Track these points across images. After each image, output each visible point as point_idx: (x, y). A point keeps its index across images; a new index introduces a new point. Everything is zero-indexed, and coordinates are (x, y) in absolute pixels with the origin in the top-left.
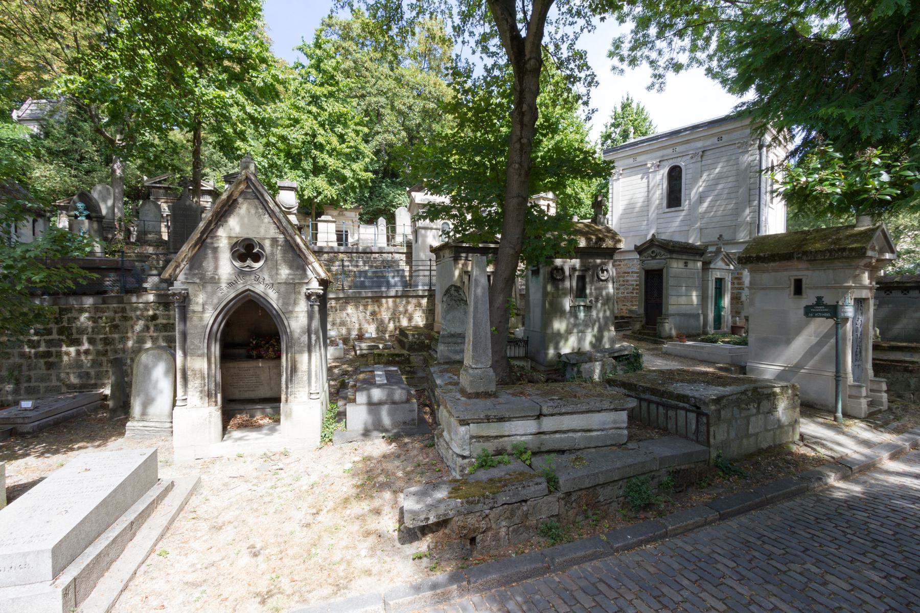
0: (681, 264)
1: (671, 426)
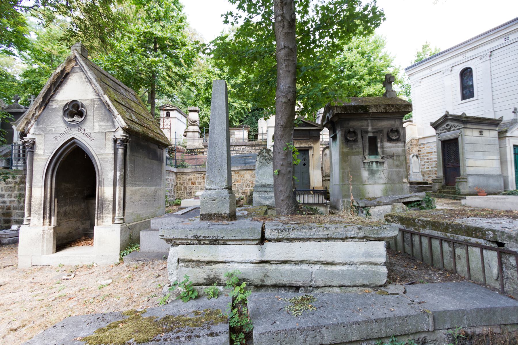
0: (476, 133)
1: (462, 267)
